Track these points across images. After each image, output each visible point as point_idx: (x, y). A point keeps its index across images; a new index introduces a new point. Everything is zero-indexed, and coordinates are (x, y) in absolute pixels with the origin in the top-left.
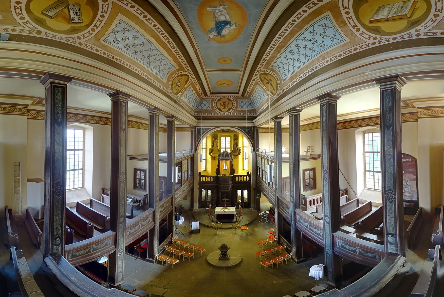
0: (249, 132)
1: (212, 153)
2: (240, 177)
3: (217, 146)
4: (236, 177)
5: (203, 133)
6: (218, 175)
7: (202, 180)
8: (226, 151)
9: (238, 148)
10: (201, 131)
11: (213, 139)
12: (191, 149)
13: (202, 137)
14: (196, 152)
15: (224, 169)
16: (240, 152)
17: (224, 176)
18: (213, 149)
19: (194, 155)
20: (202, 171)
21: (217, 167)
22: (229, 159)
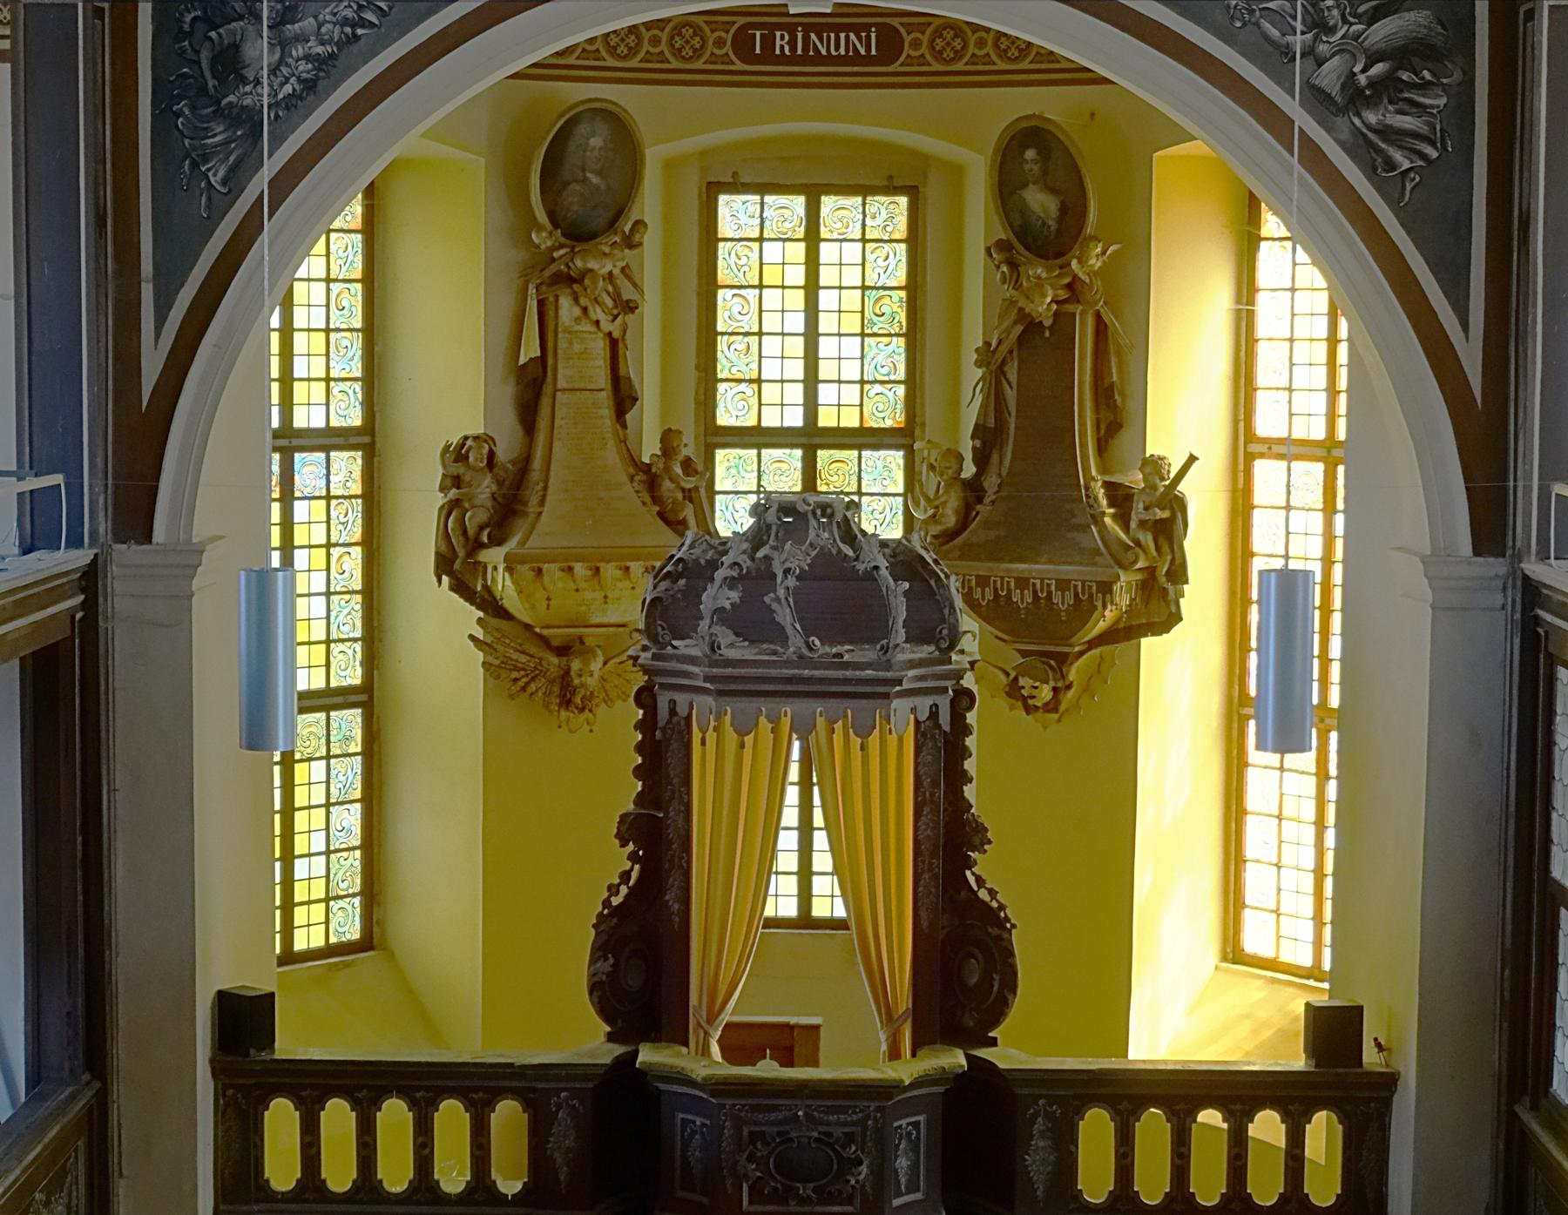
0: (1385, 89)
1: (497, 541)
2: (1153, 1125)
3: (623, 398)
4: (1079, 1113)
5: (311, 89)
6: (647, 1055)
7: (281, 1171)
8: (826, 509)
9: (1135, 479)
10: (260, 51)
11: (542, 239)
12: (33, 463)
13: (283, 185)
14: (147, 536)
15: (782, 902)
16: (1178, 574)
17: (768, 1069)
18: (524, 464)
19: (90, 606)
20: (289, 957)
21: (619, 859)
22: (878, 691)
